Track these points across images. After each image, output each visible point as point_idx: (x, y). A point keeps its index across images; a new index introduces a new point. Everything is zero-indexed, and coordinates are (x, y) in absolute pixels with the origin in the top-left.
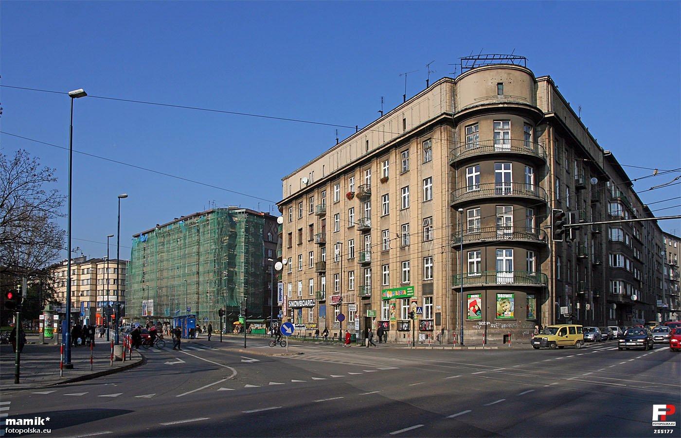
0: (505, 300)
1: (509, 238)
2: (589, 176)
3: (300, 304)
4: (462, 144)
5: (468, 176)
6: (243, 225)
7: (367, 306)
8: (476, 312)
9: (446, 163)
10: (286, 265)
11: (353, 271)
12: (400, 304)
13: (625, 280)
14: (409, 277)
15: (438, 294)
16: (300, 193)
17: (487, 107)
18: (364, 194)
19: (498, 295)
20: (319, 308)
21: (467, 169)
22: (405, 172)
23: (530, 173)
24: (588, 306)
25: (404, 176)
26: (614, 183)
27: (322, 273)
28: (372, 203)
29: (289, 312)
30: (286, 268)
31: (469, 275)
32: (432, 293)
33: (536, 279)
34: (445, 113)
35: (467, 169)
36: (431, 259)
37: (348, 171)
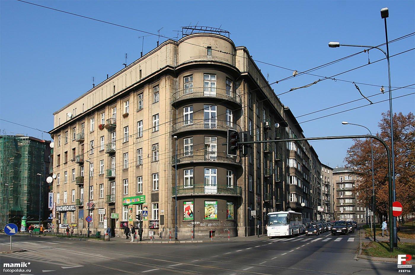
0: (211, 206)
1: (214, 160)
2: (274, 122)
3: (65, 209)
4: (181, 90)
5: (185, 114)
6: (27, 149)
7: (113, 210)
8: (189, 215)
9: (169, 103)
10: (55, 179)
11: (103, 184)
12: (136, 209)
13: (297, 193)
14: (142, 188)
15: (162, 201)
16: (66, 124)
17: (199, 63)
18: (111, 126)
19: (206, 202)
20: (78, 212)
21: (184, 109)
22: (140, 109)
23: (230, 114)
24: (272, 210)
25: (139, 112)
26: (291, 129)
27: (81, 186)
28: (117, 132)
29: (57, 215)
30: (55, 181)
31: (185, 187)
32: (158, 201)
33: (234, 190)
34: (168, 66)
35: (184, 109)
36: (158, 175)
37: (100, 108)
